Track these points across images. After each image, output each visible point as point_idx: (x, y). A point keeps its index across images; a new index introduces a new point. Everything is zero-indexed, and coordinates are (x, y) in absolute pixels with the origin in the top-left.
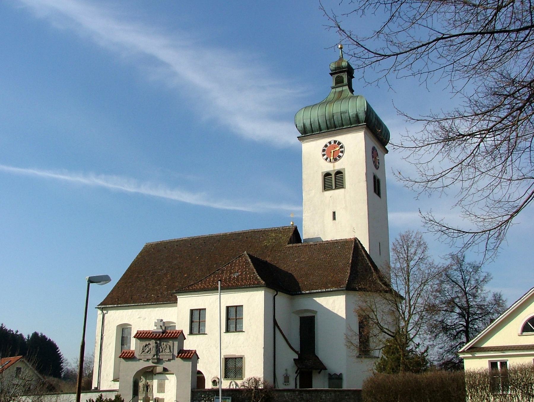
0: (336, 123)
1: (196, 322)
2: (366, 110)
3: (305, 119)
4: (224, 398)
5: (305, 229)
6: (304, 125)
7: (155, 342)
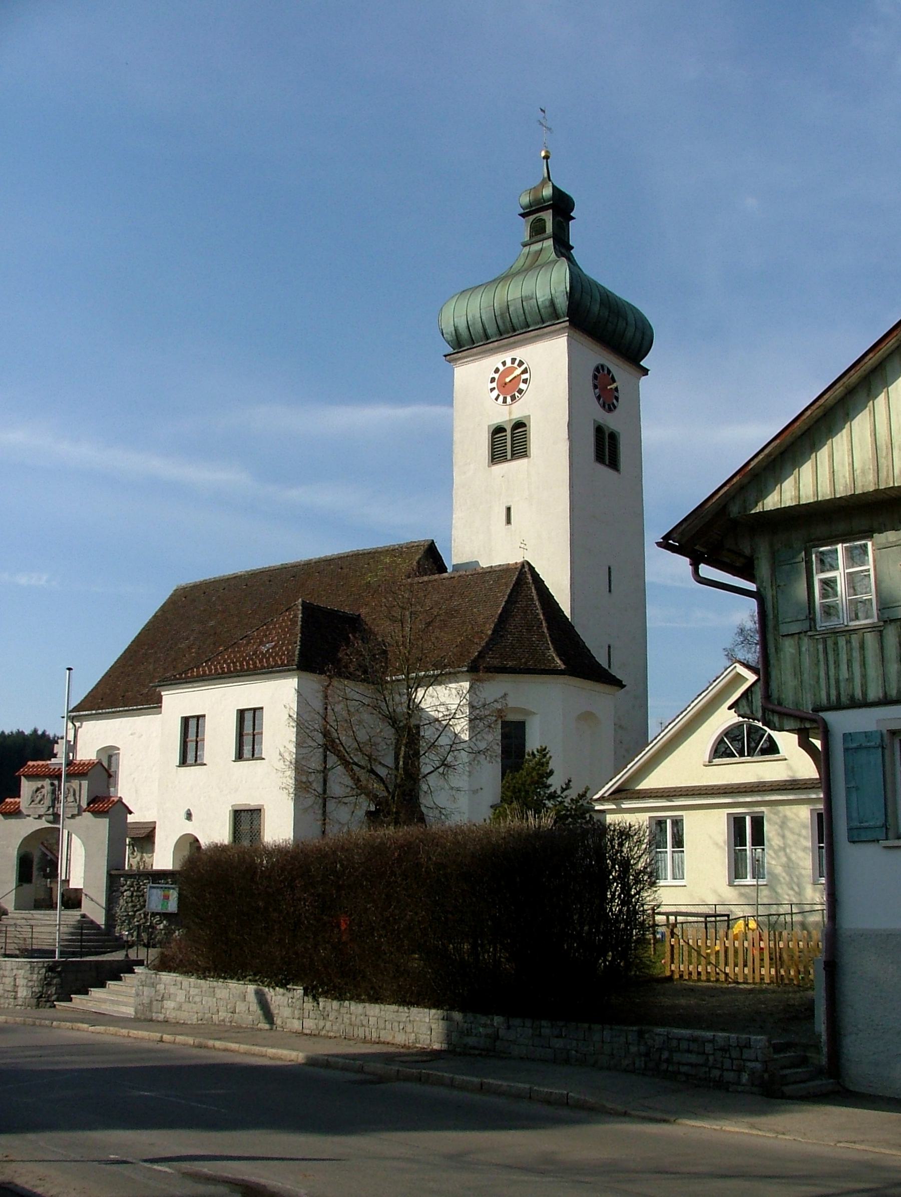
2: (568, 289)
3: (457, 317)
4: (166, 888)
5: (456, 544)
6: (456, 330)
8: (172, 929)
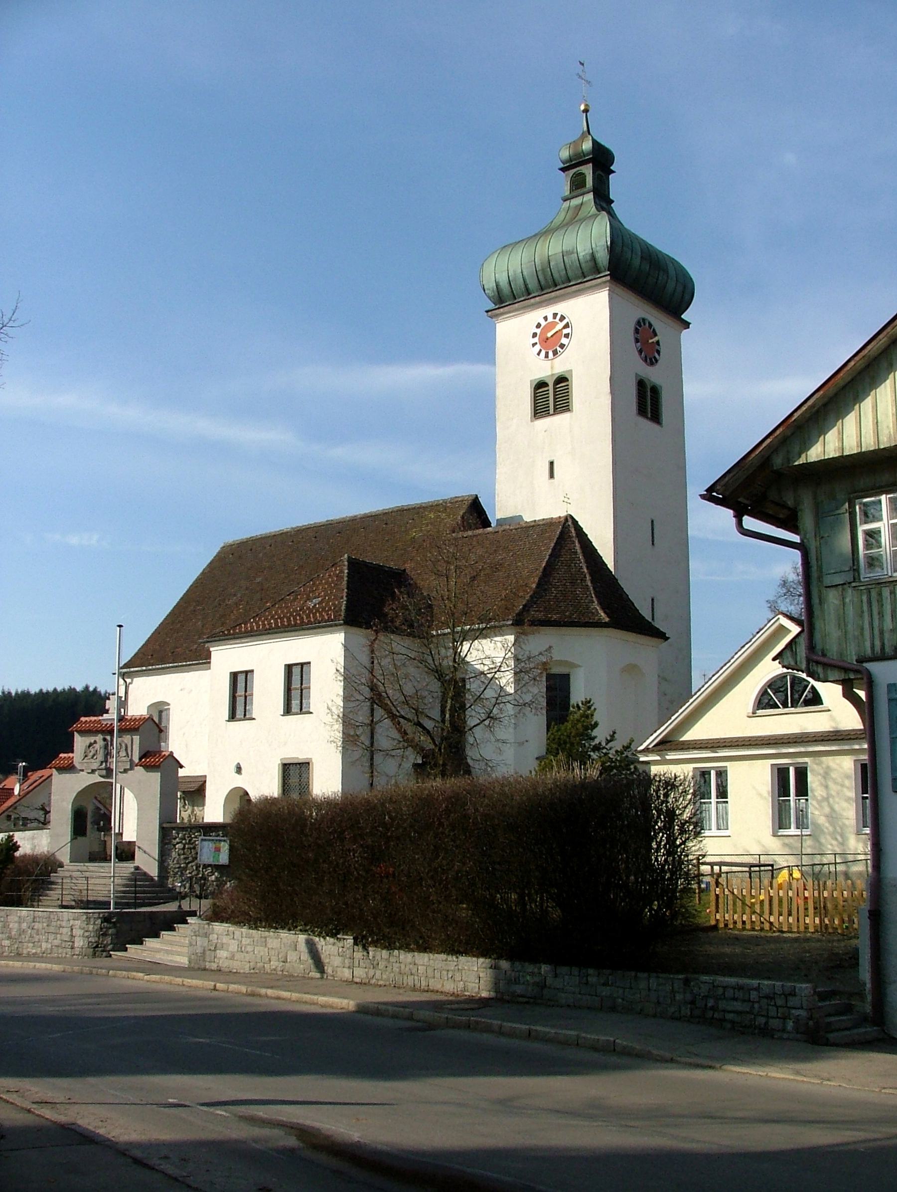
0: (556, 275)
1: (240, 696)
2: (609, 243)
4: (217, 840)
6: (497, 286)
7: (102, 737)
8: (223, 881)
